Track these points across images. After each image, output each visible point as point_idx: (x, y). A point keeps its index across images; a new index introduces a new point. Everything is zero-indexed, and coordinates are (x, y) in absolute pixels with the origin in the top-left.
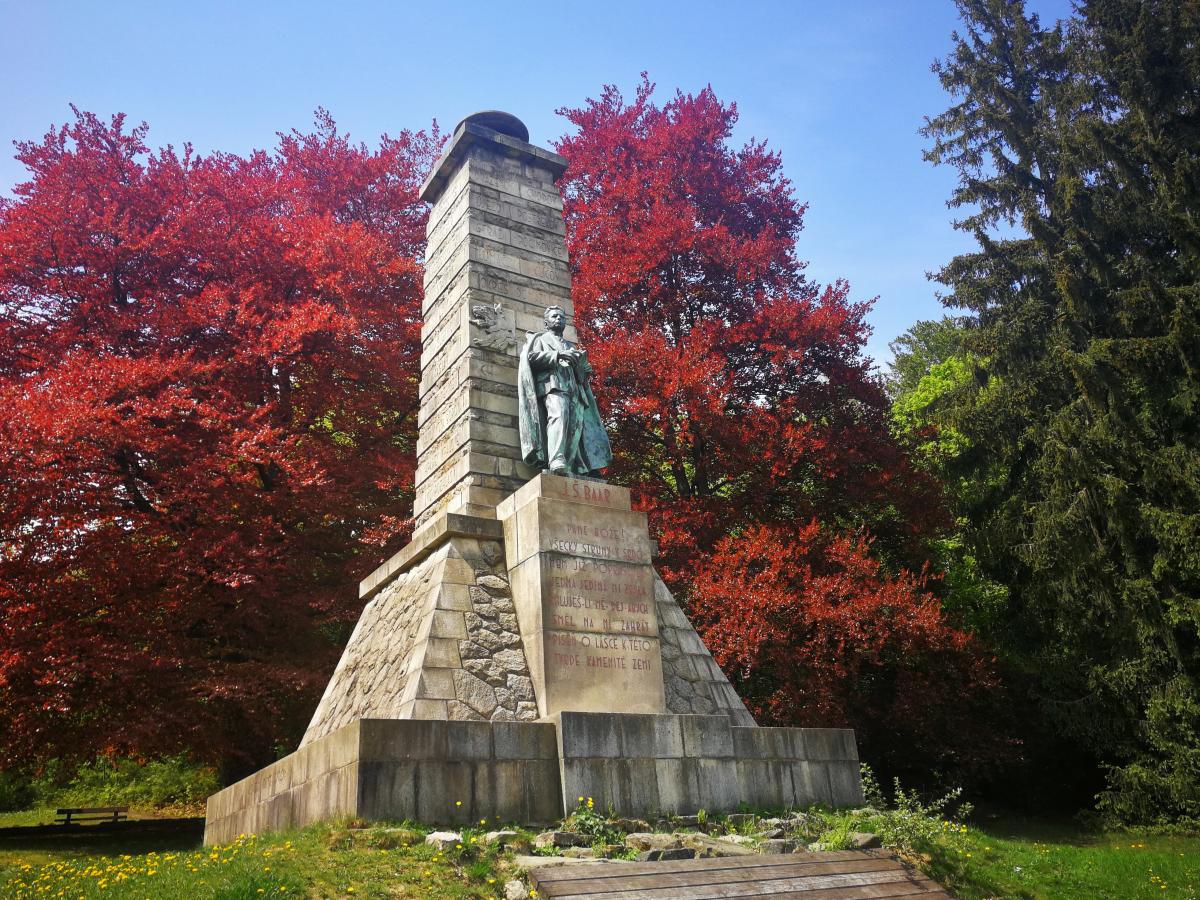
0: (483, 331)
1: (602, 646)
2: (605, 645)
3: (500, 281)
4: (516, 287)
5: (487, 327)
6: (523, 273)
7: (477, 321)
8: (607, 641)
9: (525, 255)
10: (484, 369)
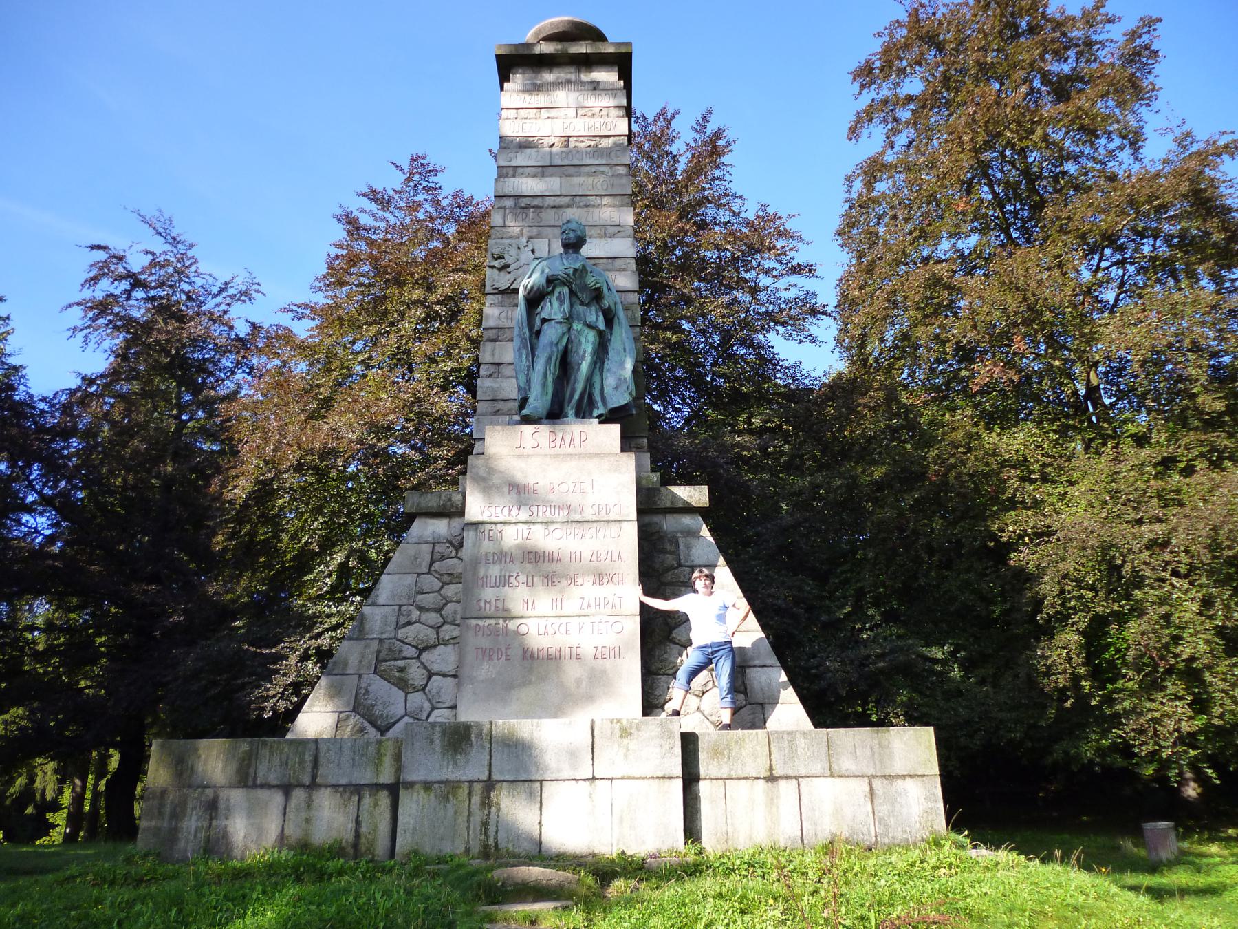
0: (502, 273)
1: (546, 632)
2: (551, 631)
3: (531, 210)
4: (554, 210)
5: (507, 266)
6: (563, 193)
7: (497, 263)
8: (556, 627)
9: (572, 170)
10: (503, 315)
